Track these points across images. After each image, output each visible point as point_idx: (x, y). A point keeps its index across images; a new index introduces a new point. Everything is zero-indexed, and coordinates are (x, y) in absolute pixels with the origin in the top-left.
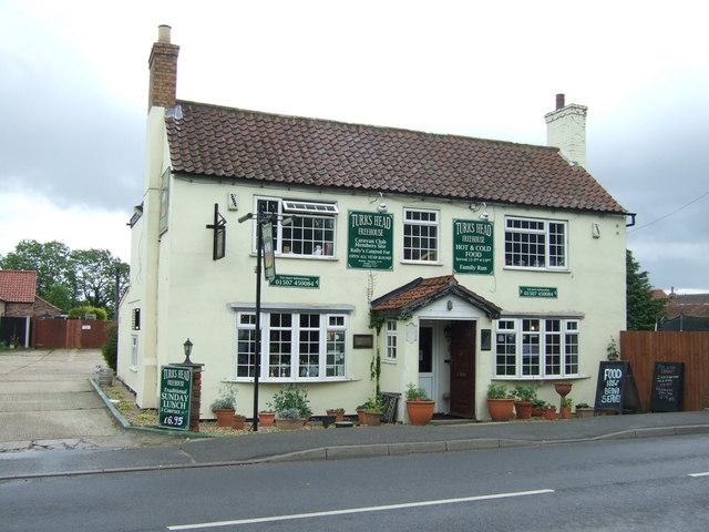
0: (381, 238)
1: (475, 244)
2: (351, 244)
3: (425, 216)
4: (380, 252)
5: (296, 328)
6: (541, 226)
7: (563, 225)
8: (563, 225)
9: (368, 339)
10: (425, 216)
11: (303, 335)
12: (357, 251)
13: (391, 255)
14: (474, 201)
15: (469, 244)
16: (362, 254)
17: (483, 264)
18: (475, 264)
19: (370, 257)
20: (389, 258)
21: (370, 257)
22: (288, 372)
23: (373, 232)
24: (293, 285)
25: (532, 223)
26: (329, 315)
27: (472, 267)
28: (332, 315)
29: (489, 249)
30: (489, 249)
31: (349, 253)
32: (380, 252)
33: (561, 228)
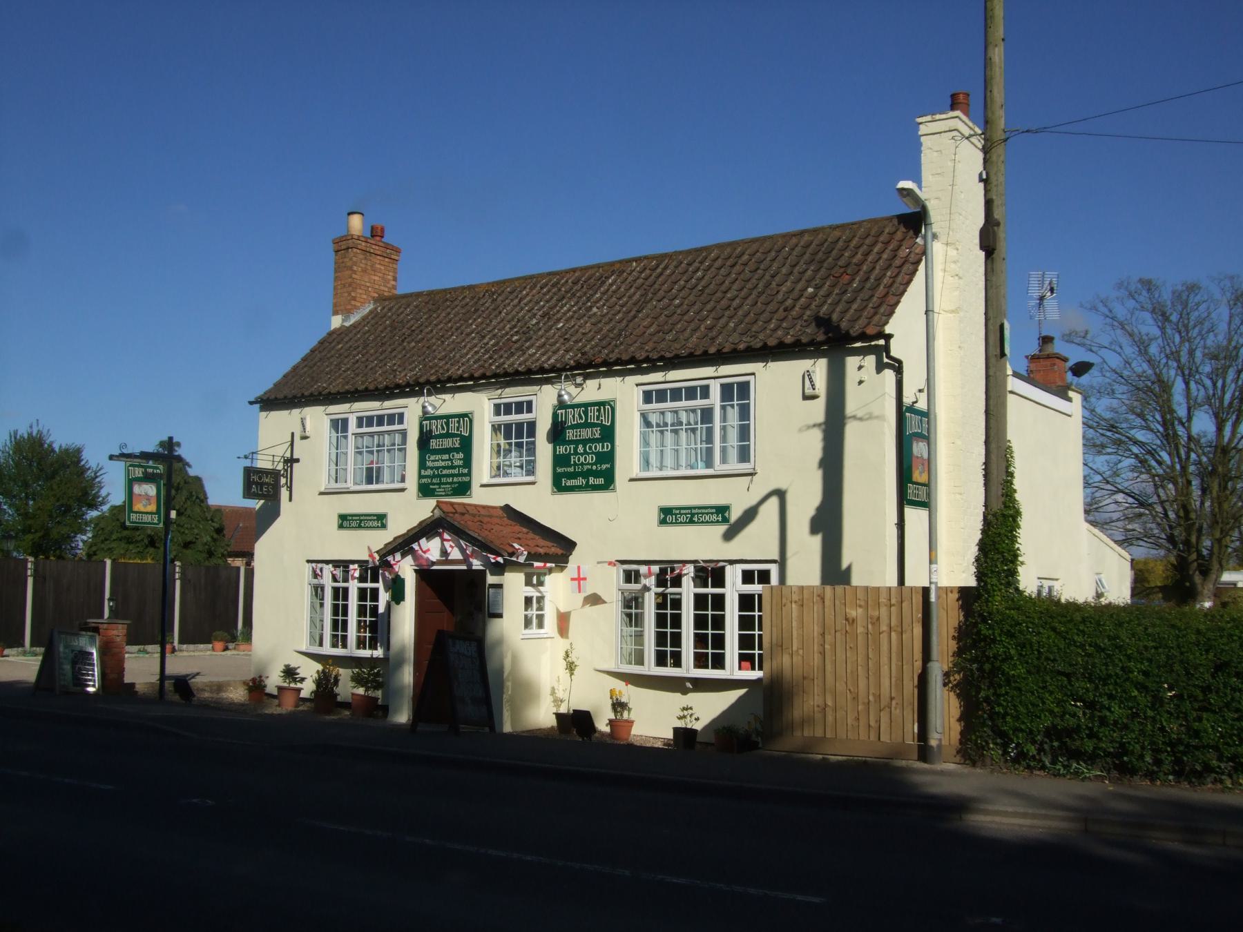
0: (457, 450)
1: (584, 442)
2: (422, 465)
3: (520, 407)
4: (456, 471)
5: (688, 591)
6: (705, 391)
7: (748, 383)
8: (748, 383)
9: (317, 587)
10: (520, 407)
11: (700, 601)
12: (429, 472)
13: (469, 474)
14: (440, 386)
15: (577, 442)
16: (434, 476)
17: (597, 474)
18: (586, 475)
19: (444, 480)
20: (559, 470)
21: (444, 480)
22: (677, 663)
23: (448, 443)
24: (691, 522)
25: (688, 389)
26: (739, 568)
27: (580, 481)
28: (627, 567)
29: (607, 447)
30: (607, 447)
31: (420, 477)
32: (456, 471)
33: (744, 389)
